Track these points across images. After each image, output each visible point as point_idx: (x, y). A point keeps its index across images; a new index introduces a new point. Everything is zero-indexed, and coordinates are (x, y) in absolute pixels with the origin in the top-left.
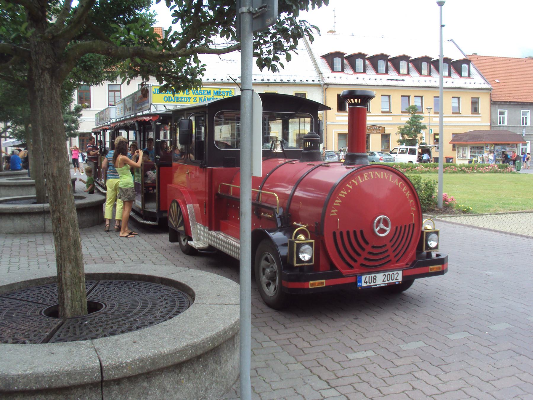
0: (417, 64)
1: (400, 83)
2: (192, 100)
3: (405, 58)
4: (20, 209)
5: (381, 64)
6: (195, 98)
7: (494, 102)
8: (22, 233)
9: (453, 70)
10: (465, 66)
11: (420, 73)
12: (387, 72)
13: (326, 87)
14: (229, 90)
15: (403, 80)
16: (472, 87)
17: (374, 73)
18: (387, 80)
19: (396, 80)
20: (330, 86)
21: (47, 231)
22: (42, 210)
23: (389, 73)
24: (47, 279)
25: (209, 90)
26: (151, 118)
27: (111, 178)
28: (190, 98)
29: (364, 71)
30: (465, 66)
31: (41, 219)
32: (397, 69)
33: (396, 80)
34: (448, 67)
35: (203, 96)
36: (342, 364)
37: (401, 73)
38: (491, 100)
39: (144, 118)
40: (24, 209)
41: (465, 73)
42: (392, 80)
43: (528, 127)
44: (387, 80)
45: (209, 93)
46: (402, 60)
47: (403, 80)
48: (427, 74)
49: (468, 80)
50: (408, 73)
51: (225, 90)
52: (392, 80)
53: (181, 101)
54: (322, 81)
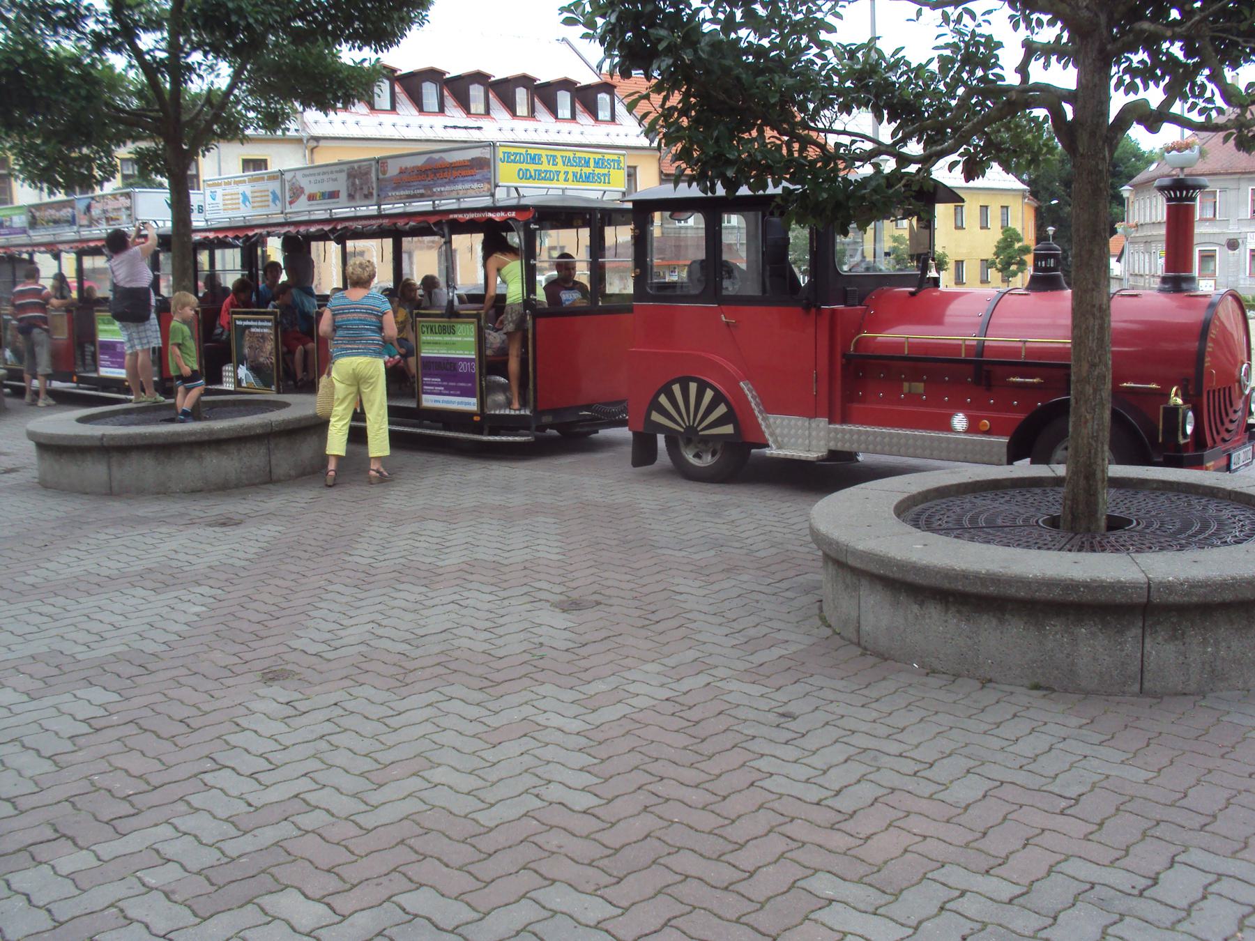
0: (504, 91)
1: (475, 136)
2: (562, 176)
3: (479, 77)
4: (222, 430)
5: (430, 92)
6: (566, 173)
7: (667, 175)
8: (224, 488)
9: (578, 107)
10: (603, 98)
11: (513, 112)
12: (442, 110)
13: (313, 144)
14: (616, 158)
15: (479, 128)
16: (623, 144)
17: (414, 112)
18: (445, 127)
19: (466, 128)
20: (322, 143)
21: (274, 477)
22: (98, 443)
23: (447, 112)
24: (1224, 490)
25: (587, 156)
26: (513, 214)
27: (343, 355)
28: (558, 173)
29: (393, 108)
30: (603, 98)
31: (263, 451)
32: (464, 104)
33: (466, 128)
34: (482, 94)
35: (577, 169)
36: (260, 776)
37: (473, 111)
38: (661, 172)
39: (490, 215)
40: (230, 429)
41: (604, 114)
42: (455, 127)
43: (733, 228)
44: (445, 127)
45: (587, 163)
46: (472, 83)
47: (479, 128)
48: (525, 114)
49: (612, 129)
50: (487, 112)
51: (611, 157)
52: (455, 127)
53: (544, 179)
54: (304, 130)
